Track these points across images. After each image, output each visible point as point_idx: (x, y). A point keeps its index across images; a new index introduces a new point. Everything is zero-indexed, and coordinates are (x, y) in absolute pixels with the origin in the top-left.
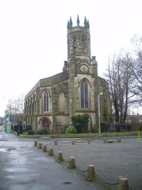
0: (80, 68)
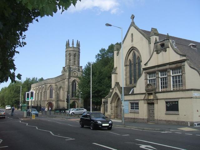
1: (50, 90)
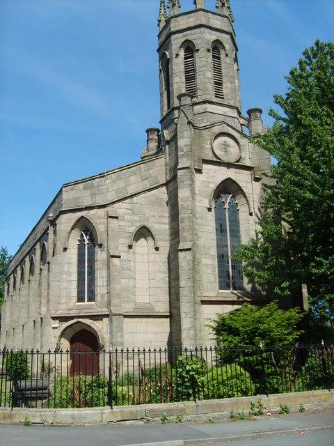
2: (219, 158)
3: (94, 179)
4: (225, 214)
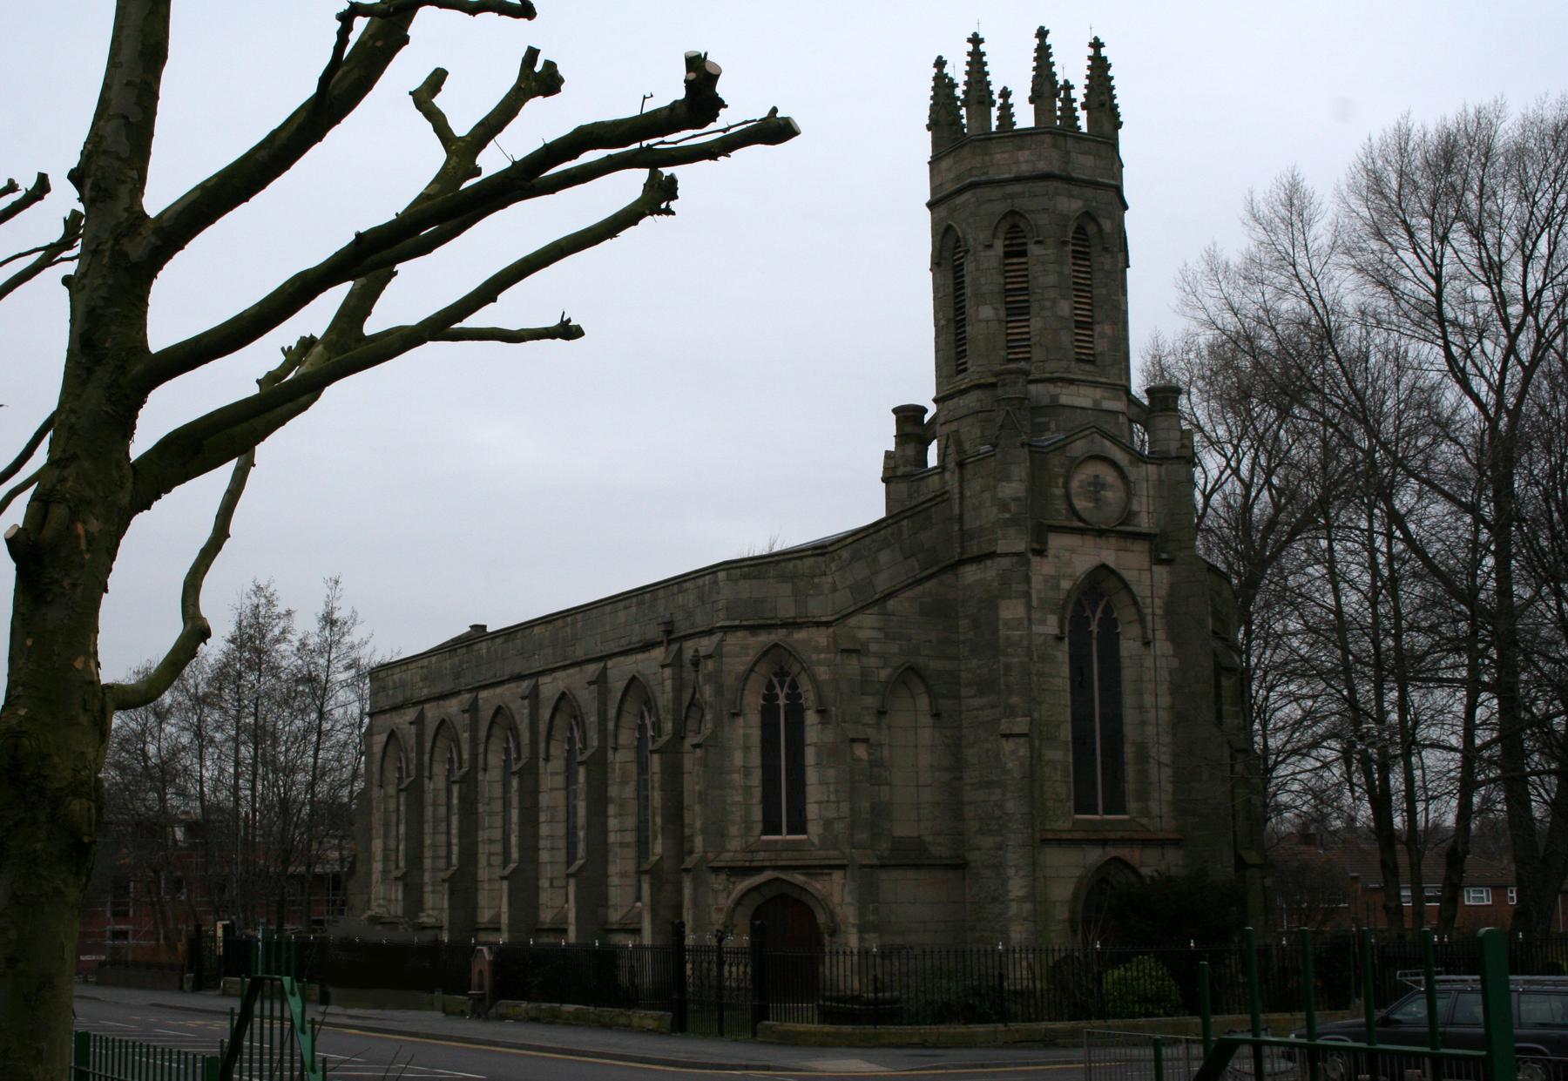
0: (1066, 486)
1: (769, 712)
2: (1081, 519)
3: (801, 558)
4: (1091, 645)
